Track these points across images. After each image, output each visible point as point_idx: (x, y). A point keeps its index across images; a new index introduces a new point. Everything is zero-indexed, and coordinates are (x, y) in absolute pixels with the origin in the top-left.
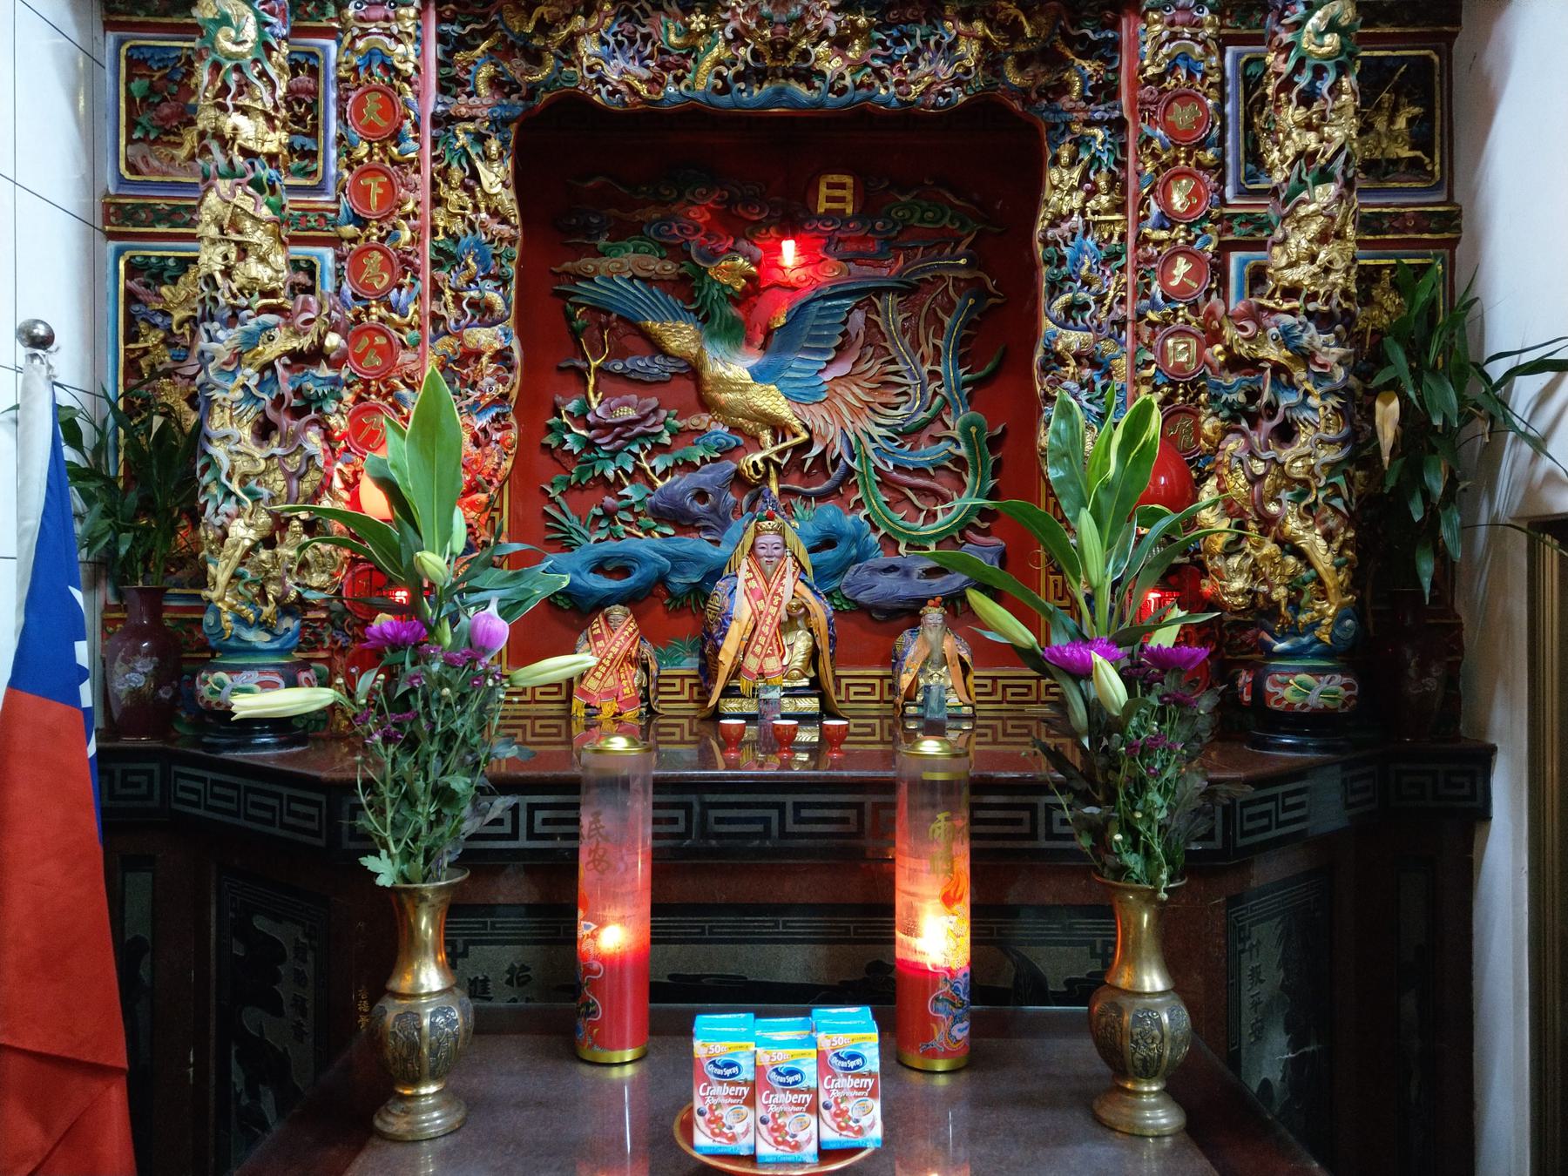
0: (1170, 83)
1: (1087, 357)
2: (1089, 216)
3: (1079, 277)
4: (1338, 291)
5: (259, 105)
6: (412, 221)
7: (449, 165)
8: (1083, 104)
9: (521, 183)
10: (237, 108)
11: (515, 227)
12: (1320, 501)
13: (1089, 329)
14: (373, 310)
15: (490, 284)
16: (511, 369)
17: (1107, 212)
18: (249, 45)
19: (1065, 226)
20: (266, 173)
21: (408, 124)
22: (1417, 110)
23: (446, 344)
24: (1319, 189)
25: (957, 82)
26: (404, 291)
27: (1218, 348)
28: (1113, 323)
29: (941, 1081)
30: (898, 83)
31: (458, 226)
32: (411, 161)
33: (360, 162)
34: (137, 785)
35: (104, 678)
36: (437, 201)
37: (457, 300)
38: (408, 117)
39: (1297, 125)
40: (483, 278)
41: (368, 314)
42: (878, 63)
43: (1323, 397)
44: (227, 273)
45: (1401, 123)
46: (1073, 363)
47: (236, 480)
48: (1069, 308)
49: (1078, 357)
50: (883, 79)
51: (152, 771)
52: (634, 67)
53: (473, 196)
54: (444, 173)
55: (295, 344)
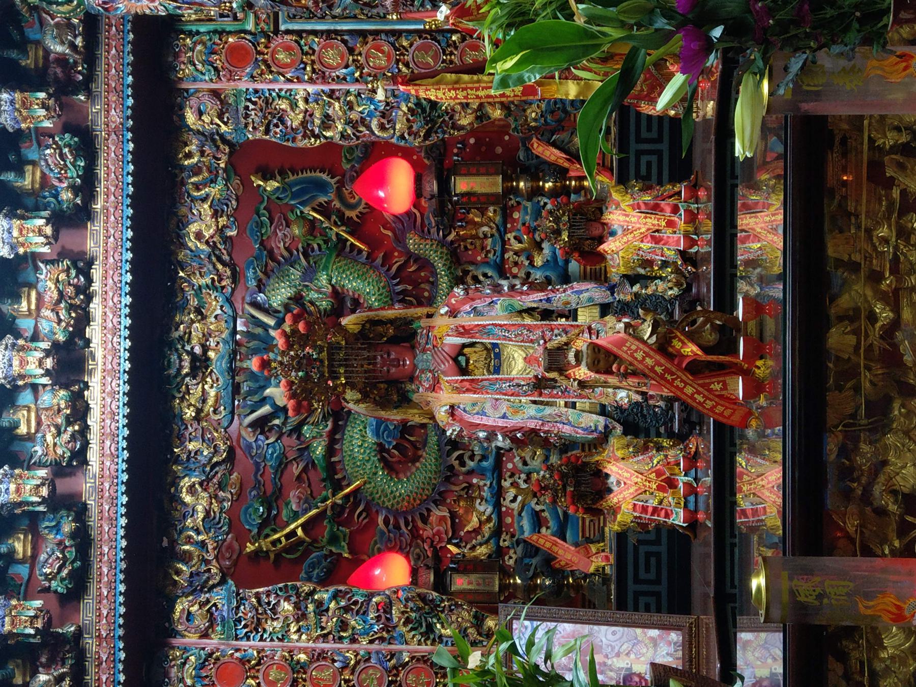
0: (218, 64)
21: (237, 655)
34: (649, 164)
35: (692, 141)
38: (232, 655)
51: (646, 553)
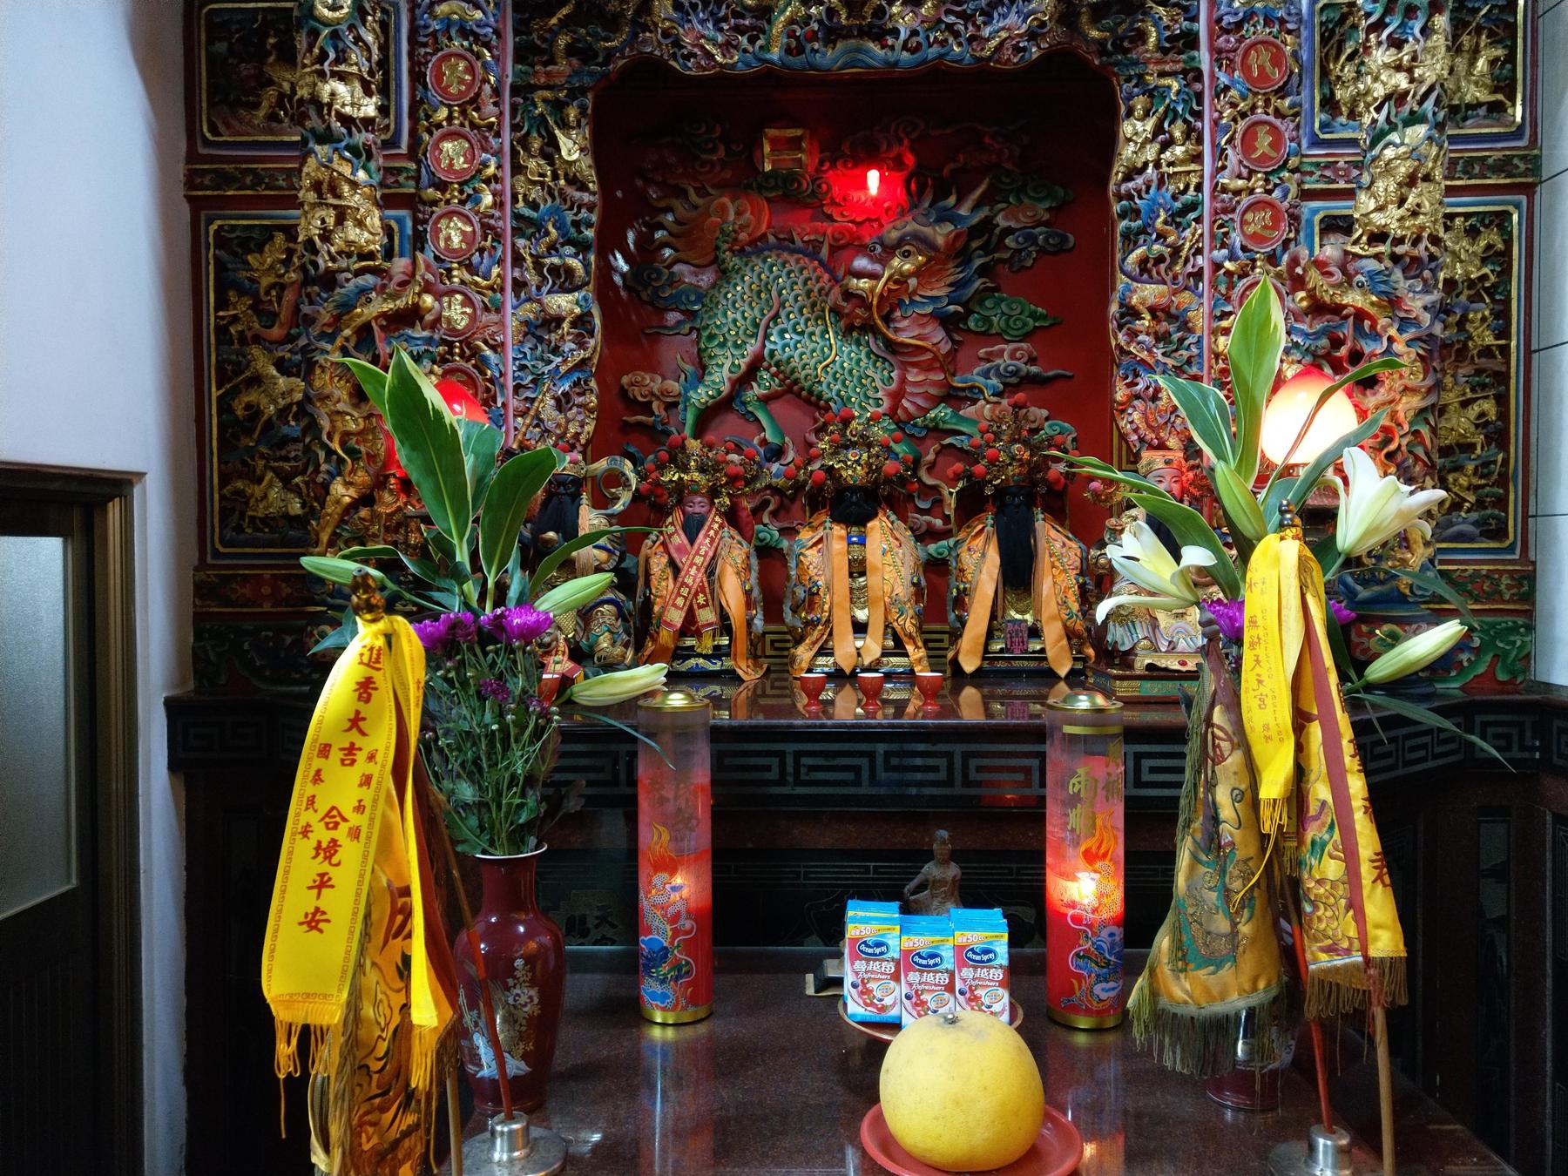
1: (1163, 310)
2: (1165, 169)
3: (1155, 229)
4: (1425, 235)
5: (354, 69)
6: (493, 185)
7: (528, 133)
8: (1158, 55)
9: (598, 148)
10: (334, 74)
11: (594, 194)
12: (1404, 448)
13: (1164, 282)
14: (455, 273)
15: (569, 250)
16: (591, 334)
17: (1183, 162)
18: (346, 10)
19: (1140, 181)
20: (362, 138)
22: (1499, 52)
23: (528, 311)
24: (1409, 131)
25: (1032, 35)
26: (486, 254)
27: (1301, 294)
28: (1190, 275)
29: (1081, 1039)
30: (971, 39)
31: (535, 193)
32: (490, 126)
33: (439, 126)
36: (517, 169)
37: (538, 266)
39: (1386, 66)
40: (563, 245)
41: (450, 277)
42: (951, 19)
43: (1409, 344)
44: (326, 237)
45: (1481, 64)
46: (1148, 317)
47: (337, 438)
48: (1143, 262)
49: (1152, 310)
50: (957, 35)
52: (709, 29)
53: (551, 164)
54: (524, 142)
55: (389, 306)
